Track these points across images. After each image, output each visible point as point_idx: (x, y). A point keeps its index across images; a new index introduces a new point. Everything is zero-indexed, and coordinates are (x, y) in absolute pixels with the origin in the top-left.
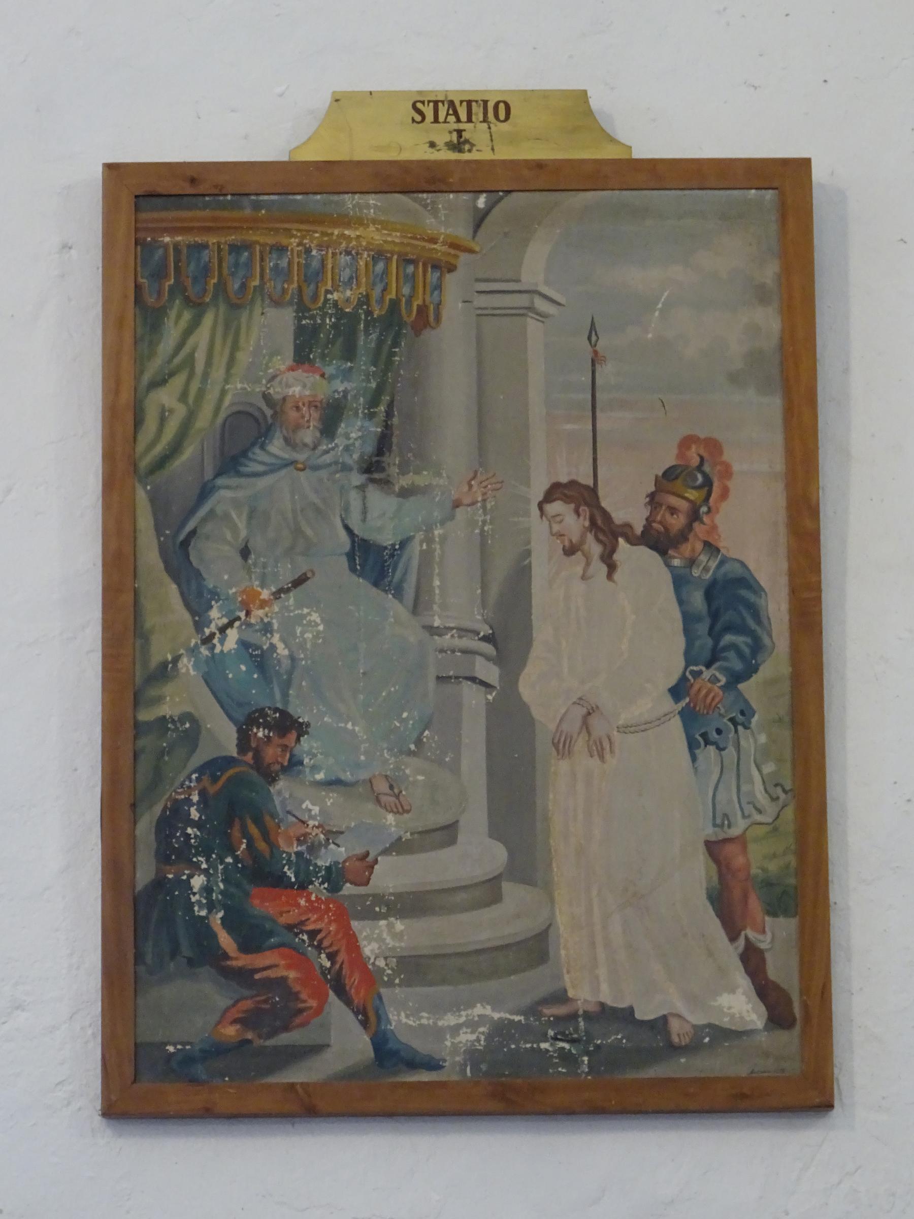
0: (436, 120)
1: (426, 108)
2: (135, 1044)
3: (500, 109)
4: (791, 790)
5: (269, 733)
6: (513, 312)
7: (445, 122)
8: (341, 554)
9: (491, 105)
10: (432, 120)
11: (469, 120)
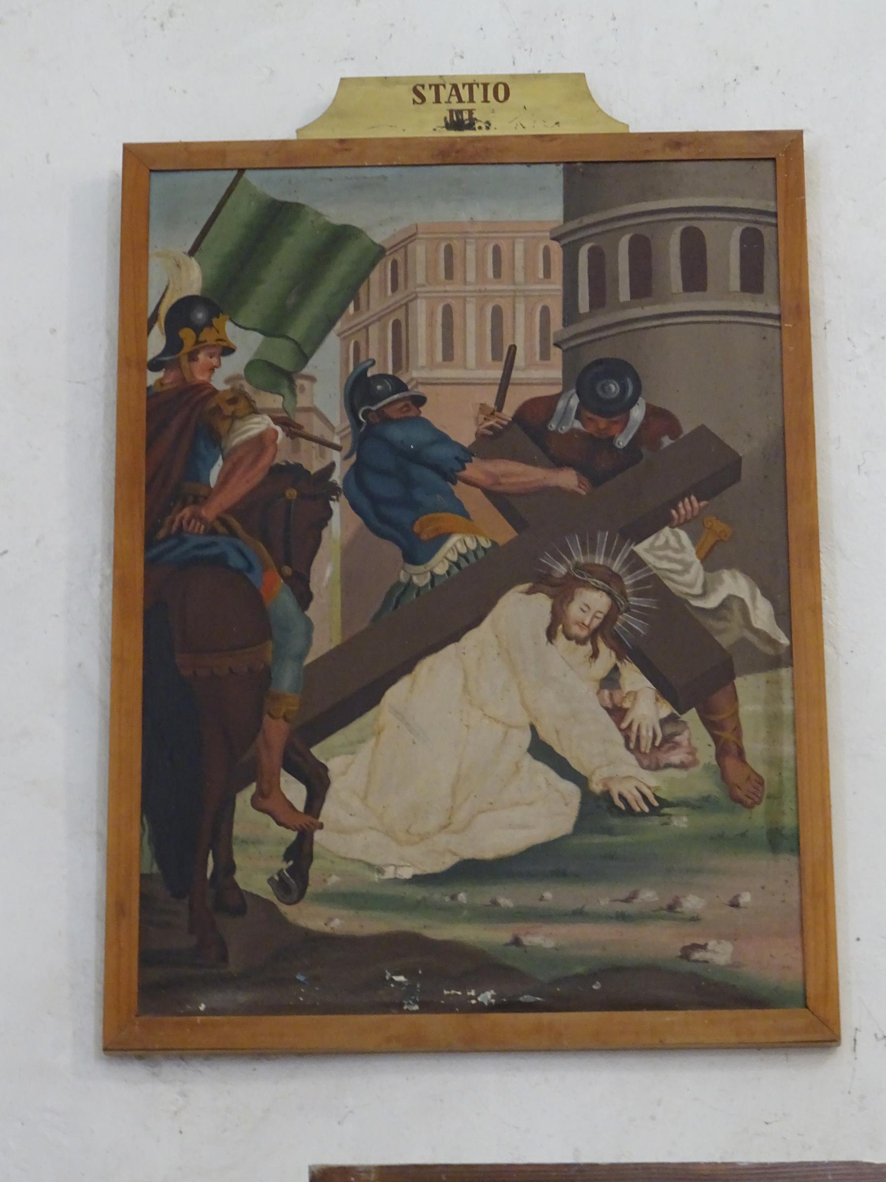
0: (438, 100)
3: (500, 89)
6: (711, 215)
7: (449, 102)
10: (434, 100)
11: (471, 100)
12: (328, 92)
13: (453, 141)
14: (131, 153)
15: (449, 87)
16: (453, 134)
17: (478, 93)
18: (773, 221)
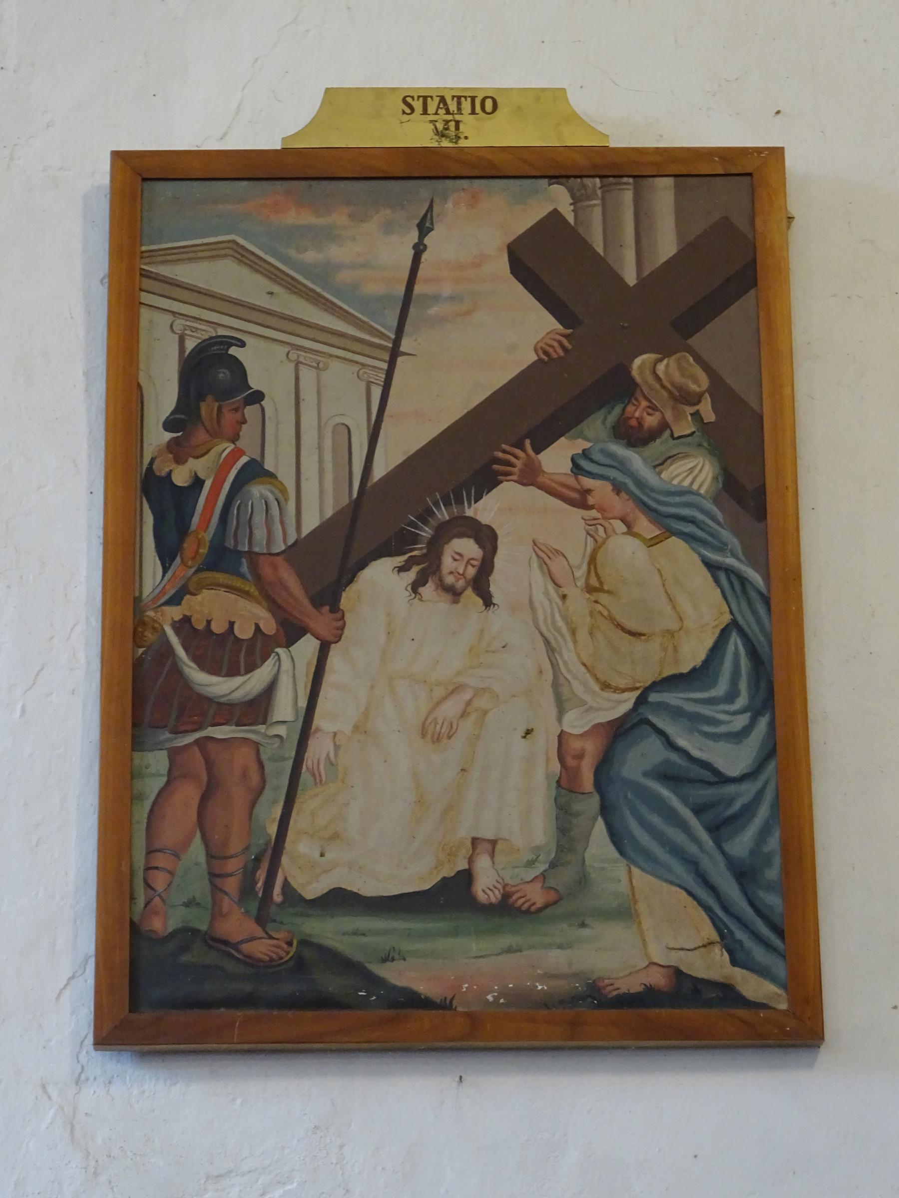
0: (425, 112)
1: (413, 103)
3: (486, 104)
4: (661, 479)
7: (436, 114)
9: (650, 543)
10: (470, 111)
11: (459, 109)
14: (123, 161)
17: (466, 105)
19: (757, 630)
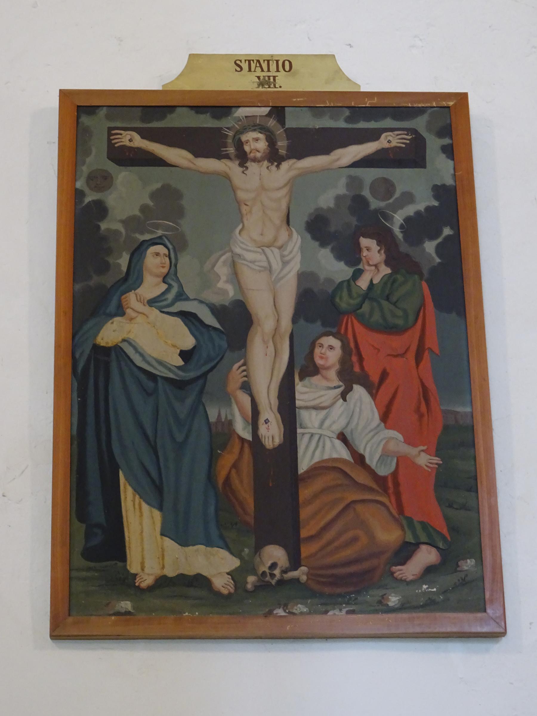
2: (284, 107)
3: (286, 64)
5: (421, 590)
8: (174, 346)
10: (248, 70)
12: (178, 65)
13: (262, 93)
15: (255, 61)
16: (261, 89)
17: (273, 67)
18: (316, 438)
19: (166, 371)
